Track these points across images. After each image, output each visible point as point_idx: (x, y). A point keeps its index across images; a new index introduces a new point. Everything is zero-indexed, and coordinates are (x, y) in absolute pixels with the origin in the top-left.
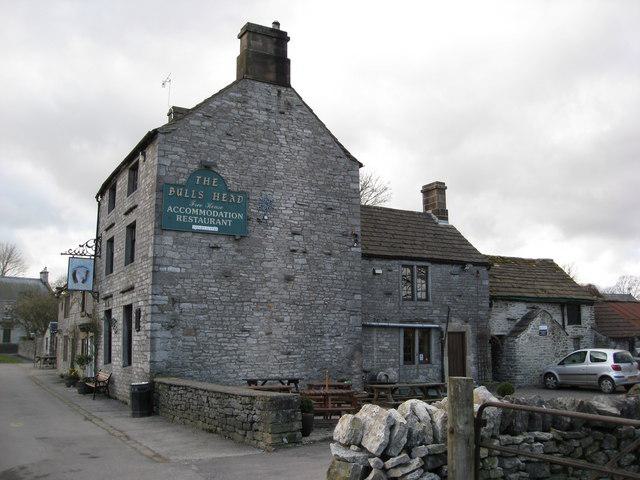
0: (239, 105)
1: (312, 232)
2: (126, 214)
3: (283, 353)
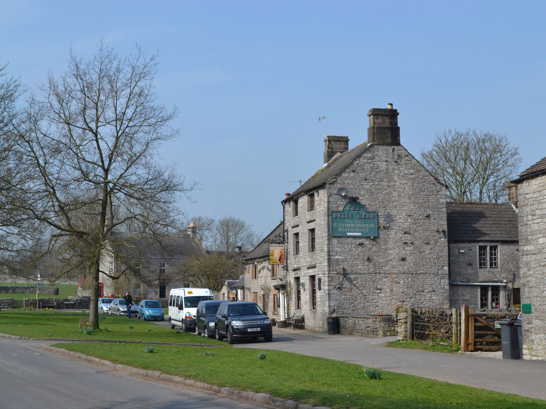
0: (370, 161)
1: (416, 231)
2: (308, 222)
3: (400, 301)
